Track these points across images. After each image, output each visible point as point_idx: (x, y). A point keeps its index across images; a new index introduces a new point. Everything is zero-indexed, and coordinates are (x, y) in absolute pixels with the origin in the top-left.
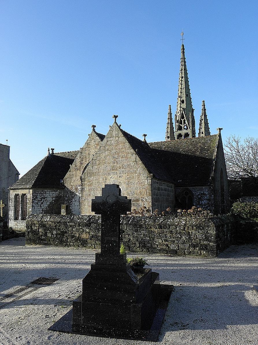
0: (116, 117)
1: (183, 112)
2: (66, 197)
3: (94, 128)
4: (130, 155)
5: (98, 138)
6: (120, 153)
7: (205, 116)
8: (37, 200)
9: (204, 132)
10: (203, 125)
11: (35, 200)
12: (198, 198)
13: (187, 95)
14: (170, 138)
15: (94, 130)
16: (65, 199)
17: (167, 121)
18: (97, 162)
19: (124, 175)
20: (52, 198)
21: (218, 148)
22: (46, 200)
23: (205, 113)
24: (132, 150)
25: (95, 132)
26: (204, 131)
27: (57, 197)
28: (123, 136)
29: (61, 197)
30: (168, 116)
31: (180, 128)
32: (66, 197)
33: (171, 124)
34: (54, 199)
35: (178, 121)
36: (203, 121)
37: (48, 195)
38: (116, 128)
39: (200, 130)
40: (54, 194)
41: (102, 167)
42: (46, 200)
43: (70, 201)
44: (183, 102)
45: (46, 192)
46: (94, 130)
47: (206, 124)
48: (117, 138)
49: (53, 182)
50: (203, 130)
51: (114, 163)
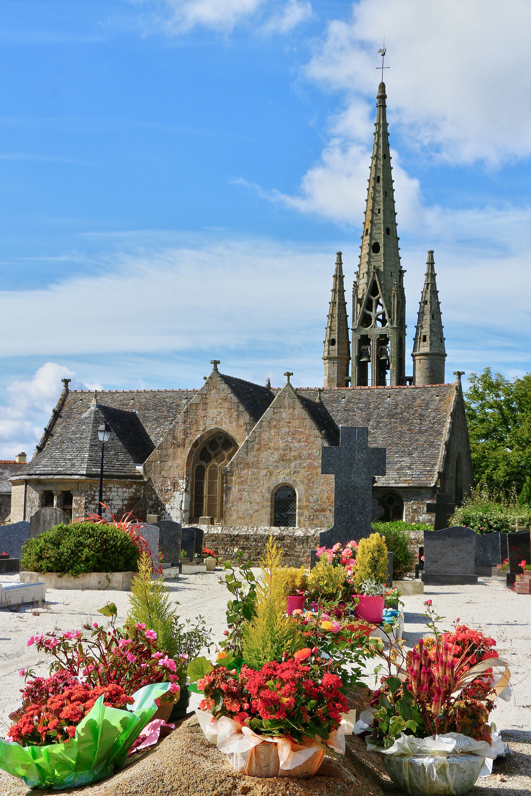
0: (289, 375)
1: (377, 279)
2: (151, 499)
3: (216, 366)
4: (312, 439)
5: (225, 386)
6: (297, 434)
7: (435, 293)
8: (94, 504)
9: (428, 338)
10: (427, 317)
11: (90, 503)
12: (412, 509)
13: (388, 231)
14: (336, 346)
15: (216, 369)
16: (146, 503)
17: (329, 296)
18: (256, 446)
19: (302, 471)
20: (123, 501)
21: (453, 415)
22: (111, 505)
23: (434, 285)
24: (317, 432)
25: (218, 373)
26: (428, 335)
27: (131, 499)
28: (302, 407)
29: (139, 498)
30: (330, 284)
31: (366, 320)
32: (151, 499)
33: (343, 304)
34: (126, 502)
35: (360, 301)
36: (428, 307)
37: (115, 494)
38: (290, 394)
39: (417, 330)
40: (126, 492)
41: (265, 454)
42: (111, 505)
43: (159, 508)
44: (375, 248)
45: (111, 488)
46: (216, 369)
47: (436, 314)
48: (291, 410)
49: (111, 468)
50: (426, 330)
51: (286, 450)
